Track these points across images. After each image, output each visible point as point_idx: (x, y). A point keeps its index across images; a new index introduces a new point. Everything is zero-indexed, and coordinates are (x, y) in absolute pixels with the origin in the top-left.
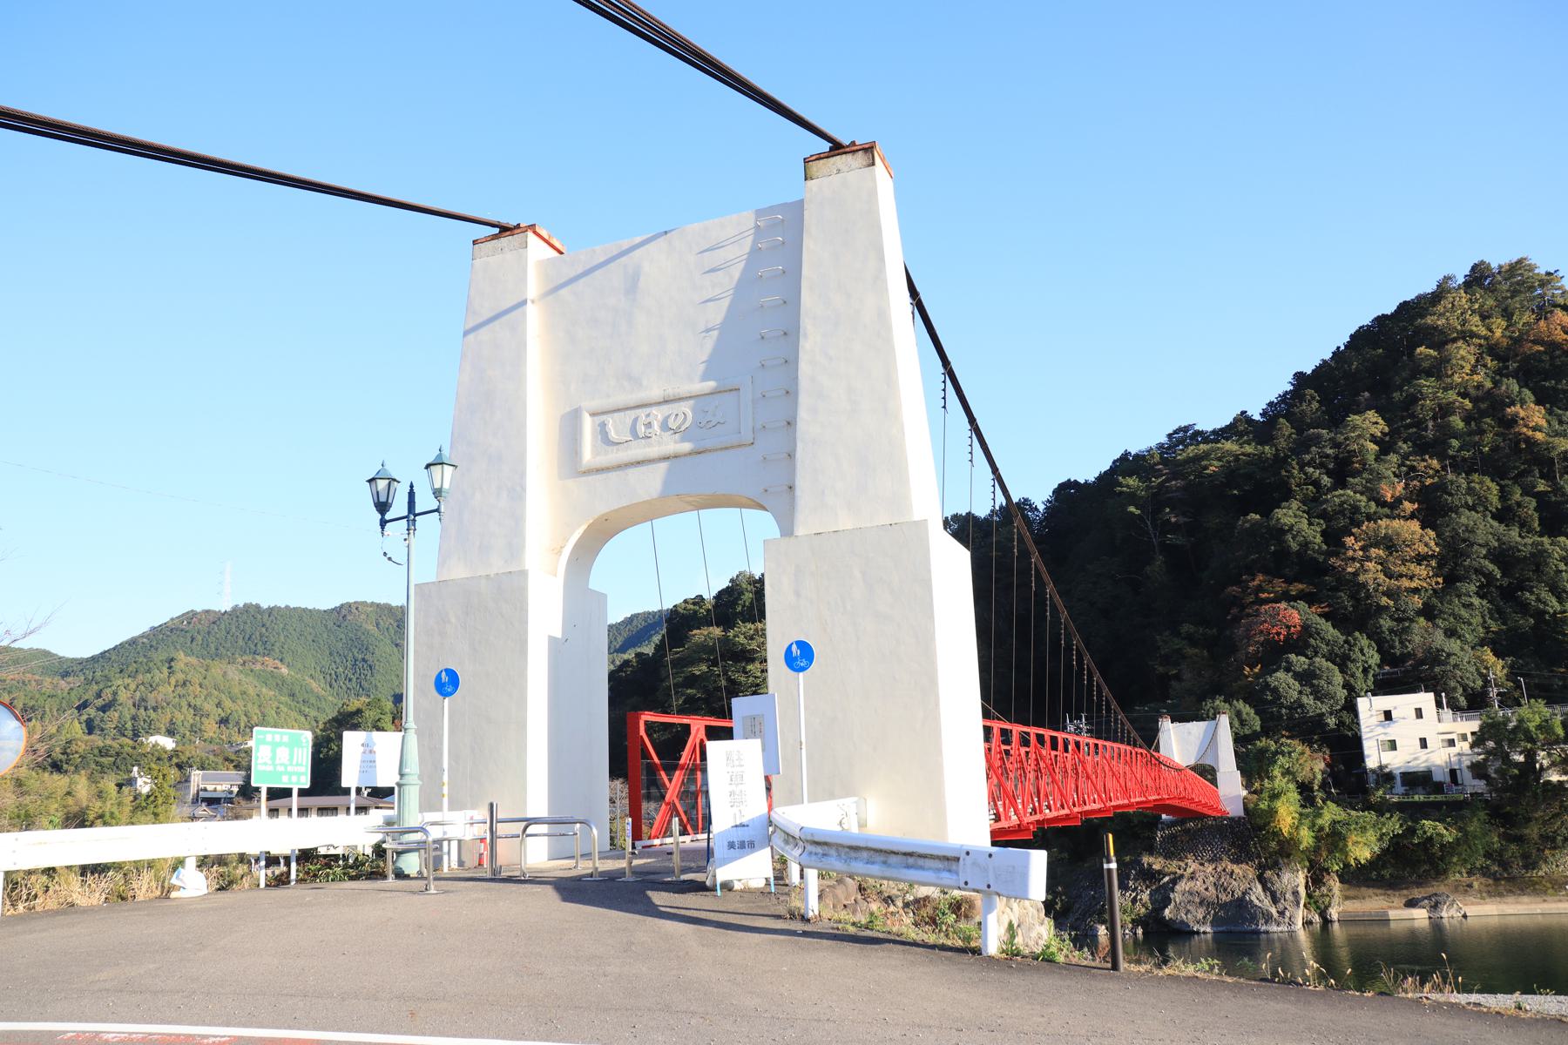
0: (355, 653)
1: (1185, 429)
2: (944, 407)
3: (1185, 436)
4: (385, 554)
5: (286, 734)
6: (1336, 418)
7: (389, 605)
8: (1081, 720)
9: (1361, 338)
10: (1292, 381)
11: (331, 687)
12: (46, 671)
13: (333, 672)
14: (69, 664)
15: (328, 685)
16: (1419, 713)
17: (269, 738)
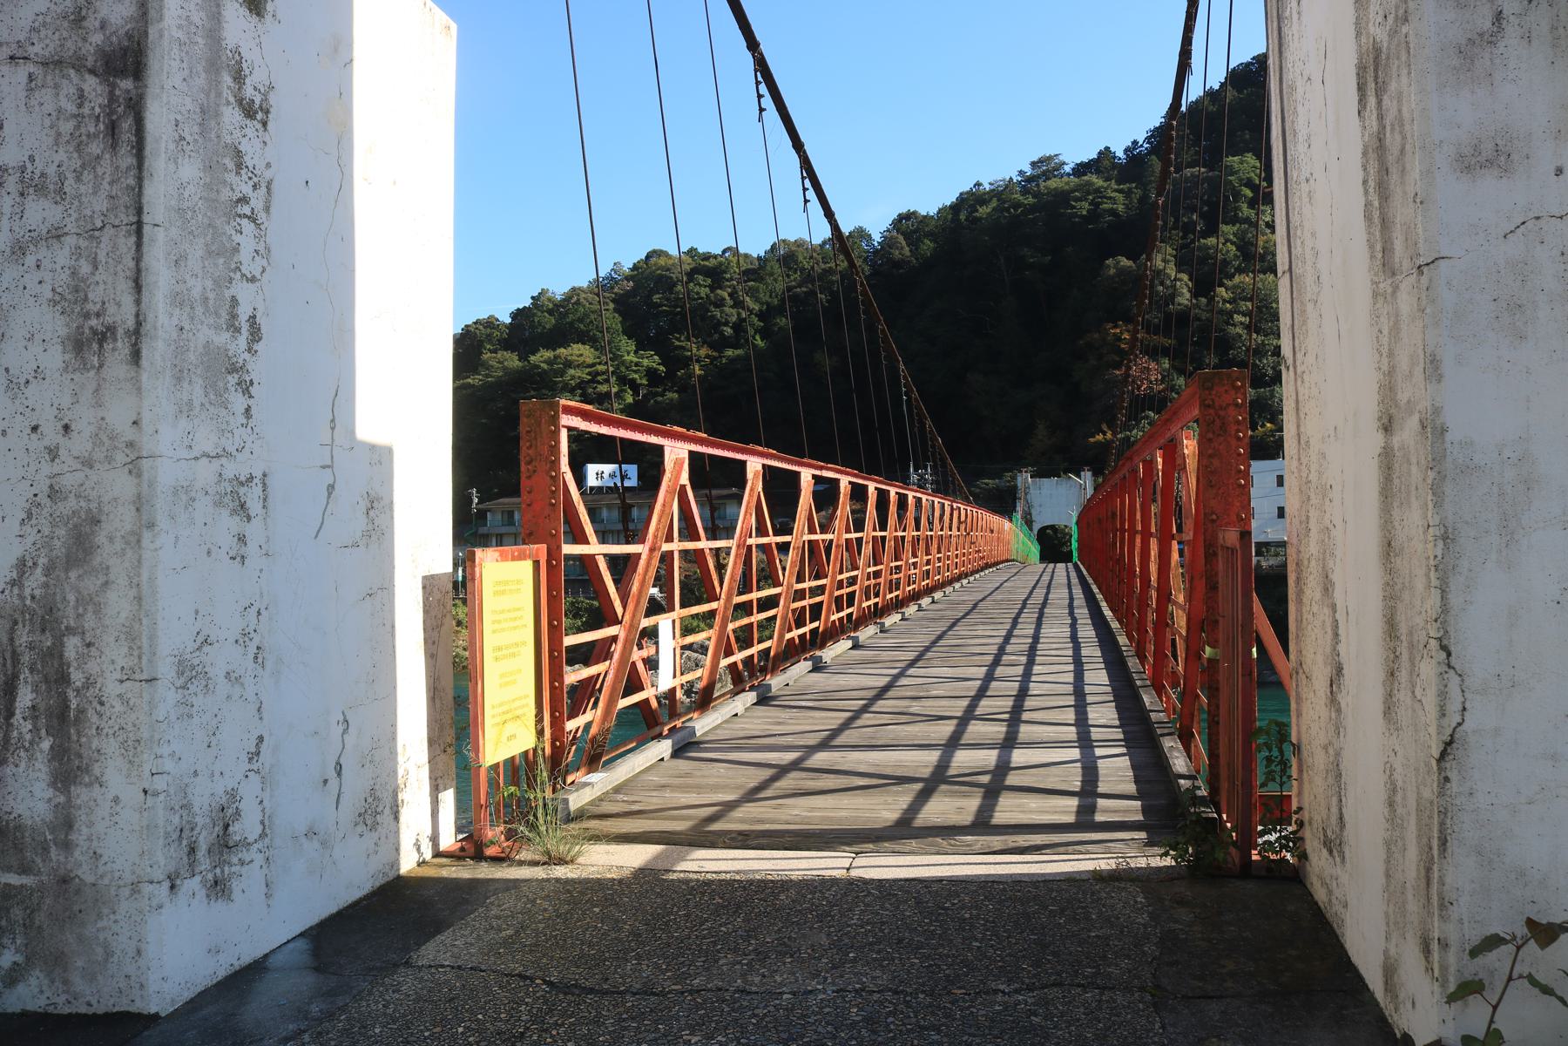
3: (1046, 167)
8: (926, 470)
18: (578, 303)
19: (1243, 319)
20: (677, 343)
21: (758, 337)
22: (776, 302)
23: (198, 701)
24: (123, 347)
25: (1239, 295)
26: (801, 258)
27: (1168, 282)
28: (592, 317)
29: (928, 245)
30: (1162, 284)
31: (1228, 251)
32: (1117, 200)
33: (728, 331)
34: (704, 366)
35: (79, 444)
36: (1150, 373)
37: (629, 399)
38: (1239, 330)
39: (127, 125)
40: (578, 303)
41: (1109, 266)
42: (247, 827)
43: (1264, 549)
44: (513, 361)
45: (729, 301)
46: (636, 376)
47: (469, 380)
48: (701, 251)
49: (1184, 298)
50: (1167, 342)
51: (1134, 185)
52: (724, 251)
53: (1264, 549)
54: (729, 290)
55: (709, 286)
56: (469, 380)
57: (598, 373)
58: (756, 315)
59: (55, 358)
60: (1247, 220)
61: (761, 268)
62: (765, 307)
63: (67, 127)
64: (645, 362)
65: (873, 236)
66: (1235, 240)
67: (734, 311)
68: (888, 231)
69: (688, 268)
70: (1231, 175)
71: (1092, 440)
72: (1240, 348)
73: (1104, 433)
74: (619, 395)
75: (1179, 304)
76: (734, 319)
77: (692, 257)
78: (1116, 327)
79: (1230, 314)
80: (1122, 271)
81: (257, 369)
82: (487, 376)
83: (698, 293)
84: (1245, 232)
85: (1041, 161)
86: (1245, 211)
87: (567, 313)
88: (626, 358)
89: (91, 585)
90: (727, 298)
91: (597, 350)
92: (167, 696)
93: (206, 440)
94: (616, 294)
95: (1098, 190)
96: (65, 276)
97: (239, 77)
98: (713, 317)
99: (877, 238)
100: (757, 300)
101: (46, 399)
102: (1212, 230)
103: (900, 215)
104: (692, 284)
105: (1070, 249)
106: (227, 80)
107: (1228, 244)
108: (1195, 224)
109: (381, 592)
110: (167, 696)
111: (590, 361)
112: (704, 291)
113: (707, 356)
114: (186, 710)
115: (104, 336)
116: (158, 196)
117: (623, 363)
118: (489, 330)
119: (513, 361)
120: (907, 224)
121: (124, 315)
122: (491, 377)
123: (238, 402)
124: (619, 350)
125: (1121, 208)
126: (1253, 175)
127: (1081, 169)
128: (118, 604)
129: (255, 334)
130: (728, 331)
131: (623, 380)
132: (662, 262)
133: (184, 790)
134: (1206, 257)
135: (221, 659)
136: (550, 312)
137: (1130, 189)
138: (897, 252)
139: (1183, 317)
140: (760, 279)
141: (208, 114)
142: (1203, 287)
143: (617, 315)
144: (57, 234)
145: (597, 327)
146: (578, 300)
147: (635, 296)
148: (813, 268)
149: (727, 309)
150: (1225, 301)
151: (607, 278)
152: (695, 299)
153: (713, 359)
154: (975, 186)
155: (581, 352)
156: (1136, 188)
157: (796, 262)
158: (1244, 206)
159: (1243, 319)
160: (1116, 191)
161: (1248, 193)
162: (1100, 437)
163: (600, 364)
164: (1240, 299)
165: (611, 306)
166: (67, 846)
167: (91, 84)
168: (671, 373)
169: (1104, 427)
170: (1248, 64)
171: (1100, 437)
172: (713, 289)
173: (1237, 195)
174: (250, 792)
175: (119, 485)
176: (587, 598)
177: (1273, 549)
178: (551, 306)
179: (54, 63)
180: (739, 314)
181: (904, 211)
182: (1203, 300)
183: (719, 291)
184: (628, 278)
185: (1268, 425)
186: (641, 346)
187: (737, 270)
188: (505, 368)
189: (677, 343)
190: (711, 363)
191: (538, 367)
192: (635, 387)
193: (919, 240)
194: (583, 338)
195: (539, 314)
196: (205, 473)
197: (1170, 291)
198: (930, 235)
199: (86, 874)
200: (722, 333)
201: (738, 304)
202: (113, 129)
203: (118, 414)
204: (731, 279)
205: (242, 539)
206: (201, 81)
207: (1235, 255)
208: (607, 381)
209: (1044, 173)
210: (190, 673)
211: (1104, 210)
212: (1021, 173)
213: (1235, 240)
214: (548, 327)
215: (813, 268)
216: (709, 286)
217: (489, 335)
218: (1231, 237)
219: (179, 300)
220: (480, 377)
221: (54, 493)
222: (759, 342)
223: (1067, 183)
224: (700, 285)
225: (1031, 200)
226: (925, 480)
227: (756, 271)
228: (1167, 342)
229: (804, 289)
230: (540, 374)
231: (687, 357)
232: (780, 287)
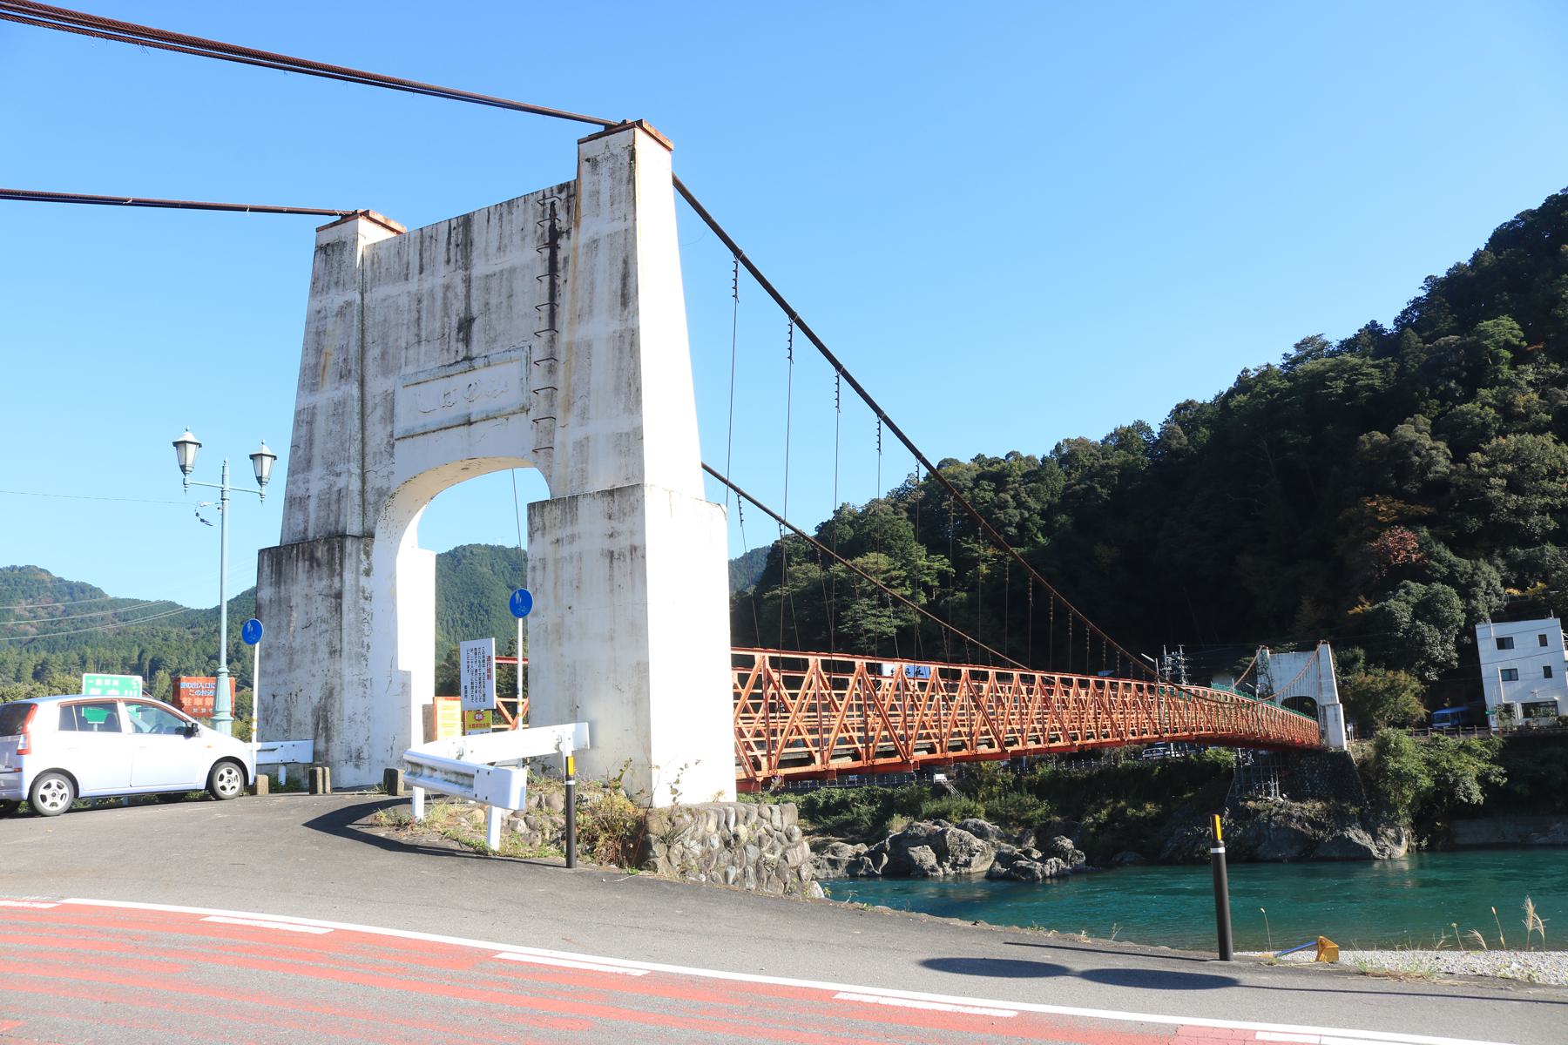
0: (471, 597)
1: (1311, 340)
2: (790, 358)
3: (1310, 348)
4: (197, 515)
5: (116, 679)
6: (1466, 324)
7: (503, 547)
8: (1179, 652)
9: (1503, 238)
10: (1423, 285)
11: (448, 633)
12: (172, 621)
13: (449, 618)
14: (195, 616)
15: (445, 631)
16: (1543, 640)
17: (99, 682)
18: (874, 514)
19: (1500, 482)
20: (966, 546)
21: (1039, 535)
22: (1056, 500)
23: (353, 726)
24: (338, 654)
25: (1499, 457)
26: (1081, 457)
27: (1424, 452)
28: (887, 526)
29: (1204, 433)
30: (1418, 454)
31: (1487, 415)
32: (1374, 376)
33: (1012, 530)
34: (990, 565)
35: (331, 673)
36: (1406, 543)
37: (924, 601)
38: (1495, 493)
39: (339, 609)
40: (874, 514)
41: (1363, 442)
42: (365, 755)
43: (1533, 711)
44: (815, 571)
45: (1012, 503)
46: (928, 579)
47: (778, 592)
48: (988, 457)
49: (1443, 465)
50: (1426, 510)
51: (1390, 359)
52: (1007, 456)
53: (1533, 711)
54: (1012, 493)
55: (994, 490)
56: (778, 592)
57: (892, 579)
58: (1038, 514)
59: (327, 655)
60: (1508, 382)
61: (1042, 467)
62: (1046, 506)
63: (329, 609)
64: (936, 565)
65: (1153, 429)
66: (1494, 402)
67: (1017, 512)
68: (1167, 422)
69: (974, 474)
70: (1487, 339)
71: (1351, 612)
72: (1501, 510)
73: (1363, 604)
74: (912, 597)
75: (1436, 472)
76: (1017, 519)
77: (979, 464)
78: (1372, 501)
79: (1487, 478)
80: (1377, 446)
81: (369, 655)
82: (793, 587)
83: (983, 498)
84: (1505, 394)
85: (1304, 342)
86: (1506, 372)
87: (864, 524)
88: (919, 562)
89: (333, 701)
90: (1010, 500)
91: (891, 556)
92: (346, 723)
93: (356, 671)
94: (909, 503)
95: (1353, 368)
96: (328, 640)
97: (364, 592)
98: (997, 519)
99: (1156, 430)
100: (1038, 500)
101: (325, 664)
102: (1471, 396)
103: (1177, 406)
104: (977, 490)
105: (1329, 428)
106: (361, 594)
107: (1487, 407)
108: (1453, 391)
109: (406, 708)
110: (346, 723)
111: (884, 567)
112: (989, 495)
113: (994, 556)
114: (350, 727)
115: (335, 651)
116: (345, 622)
117: (915, 567)
118: (796, 544)
119: (815, 571)
120: (1186, 414)
121: (338, 647)
122: (798, 587)
123: (364, 663)
124: (911, 555)
125: (1377, 382)
126: (1510, 336)
127: (1349, 345)
128: (337, 705)
129: (369, 647)
130: (1012, 530)
131: (918, 584)
132: (951, 470)
133: (349, 744)
134: (1464, 421)
135: (358, 718)
136: (851, 524)
137: (1386, 364)
138: (1175, 442)
139: (1442, 485)
140: (1042, 480)
141: (356, 602)
142: (1459, 454)
143: (910, 523)
144: (327, 631)
145: (892, 535)
146: (875, 511)
147: (927, 504)
148: (1093, 464)
149: (1010, 511)
150: (1480, 466)
151: (903, 489)
152: (982, 504)
153: (1000, 558)
154: (1242, 373)
155: (876, 560)
156: (1393, 361)
157: (1077, 460)
158: (1505, 368)
159: (1500, 482)
160: (1373, 366)
161: (1507, 354)
162: (1358, 609)
163: (894, 569)
164: (1500, 461)
165: (905, 515)
166: (327, 755)
167: (333, 600)
168: (960, 575)
169: (1362, 598)
170: (1512, 223)
171: (1358, 609)
172: (997, 491)
173: (1497, 359)
174: (366, 748)
175: (337, 681)
176: (881, 786)
177: (1542, 709)
178: (851, 518)
179: (327, 596)
180: (1022, 514)
181: (1183, 401)
182: (1463, 466)
183: (1002, 495)
184: (923, 487)
185: (1539, 584)
186: (932, 550)
187: (1020, 473)
188: (809, 579)
189: (966, 546)
190: (998, 562)
191: (837, 576)
192: (928, 589)
193: (1196, 428)
194: (886, 549)
195: (841, 526)
196: (356, 678)
197: (1427, 459)
198: (1208, 422)
199: (331, 761)
200: (1006, 533)
201: (1020, 505)
202: (336, 610)
203: (337, 667)
204: (1014, 482)
205: (365, 693)
206: (354, 596)
207: (1494, 418)
208: (902, 584)
209: (1309, 354)
210: (351, 720)
211: (1361, 386)
212: (1286, 356)
213: (1494, 402)
214: (847, 538)
215: (1093, 464)
216: (994, 490)
217: (796, 549)
218: (1491, 400)
219: (349, 643)
220: (787, 588)
221: (326, 683)
222: (1041, 539)
223: (1323, 364)
224: (985, 490)
225: (1287, 384)
226: (1179, 661)
227: (1036, 473)
228: (1426, 510)
229: (1083, 486)
230: (839, 582)
231: (975, 557)
232: (1061, 483)
